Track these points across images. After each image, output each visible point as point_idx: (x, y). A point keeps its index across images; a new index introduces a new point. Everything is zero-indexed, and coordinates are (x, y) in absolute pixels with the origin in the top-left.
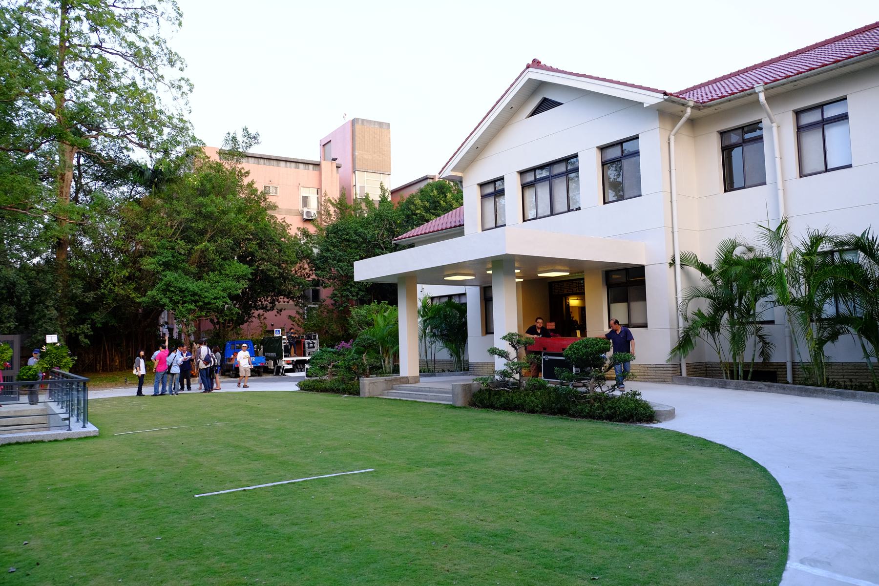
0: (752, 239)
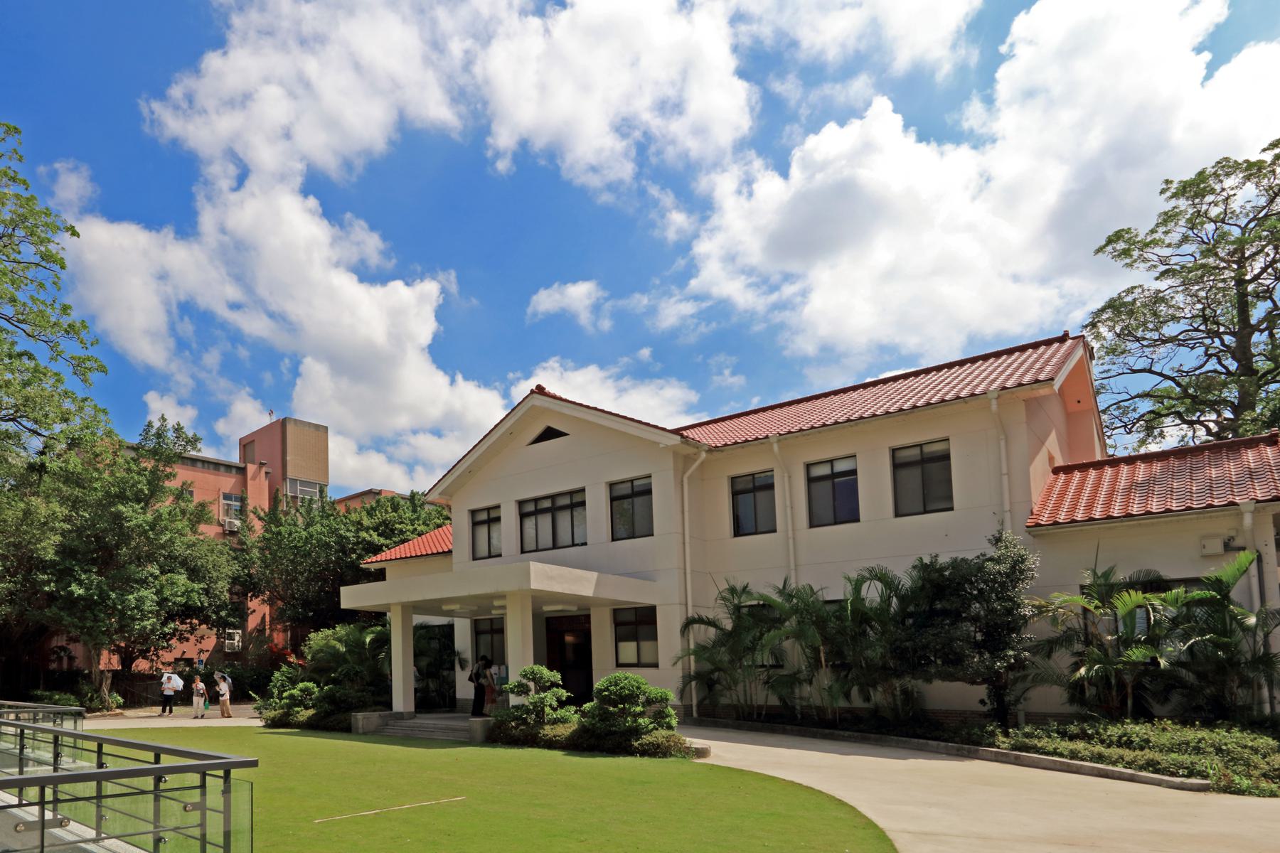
0: (765, 586)
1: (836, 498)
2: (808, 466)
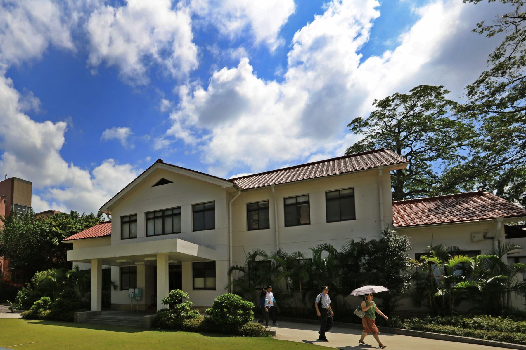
1: (297, 213)
2: (285, 199)
